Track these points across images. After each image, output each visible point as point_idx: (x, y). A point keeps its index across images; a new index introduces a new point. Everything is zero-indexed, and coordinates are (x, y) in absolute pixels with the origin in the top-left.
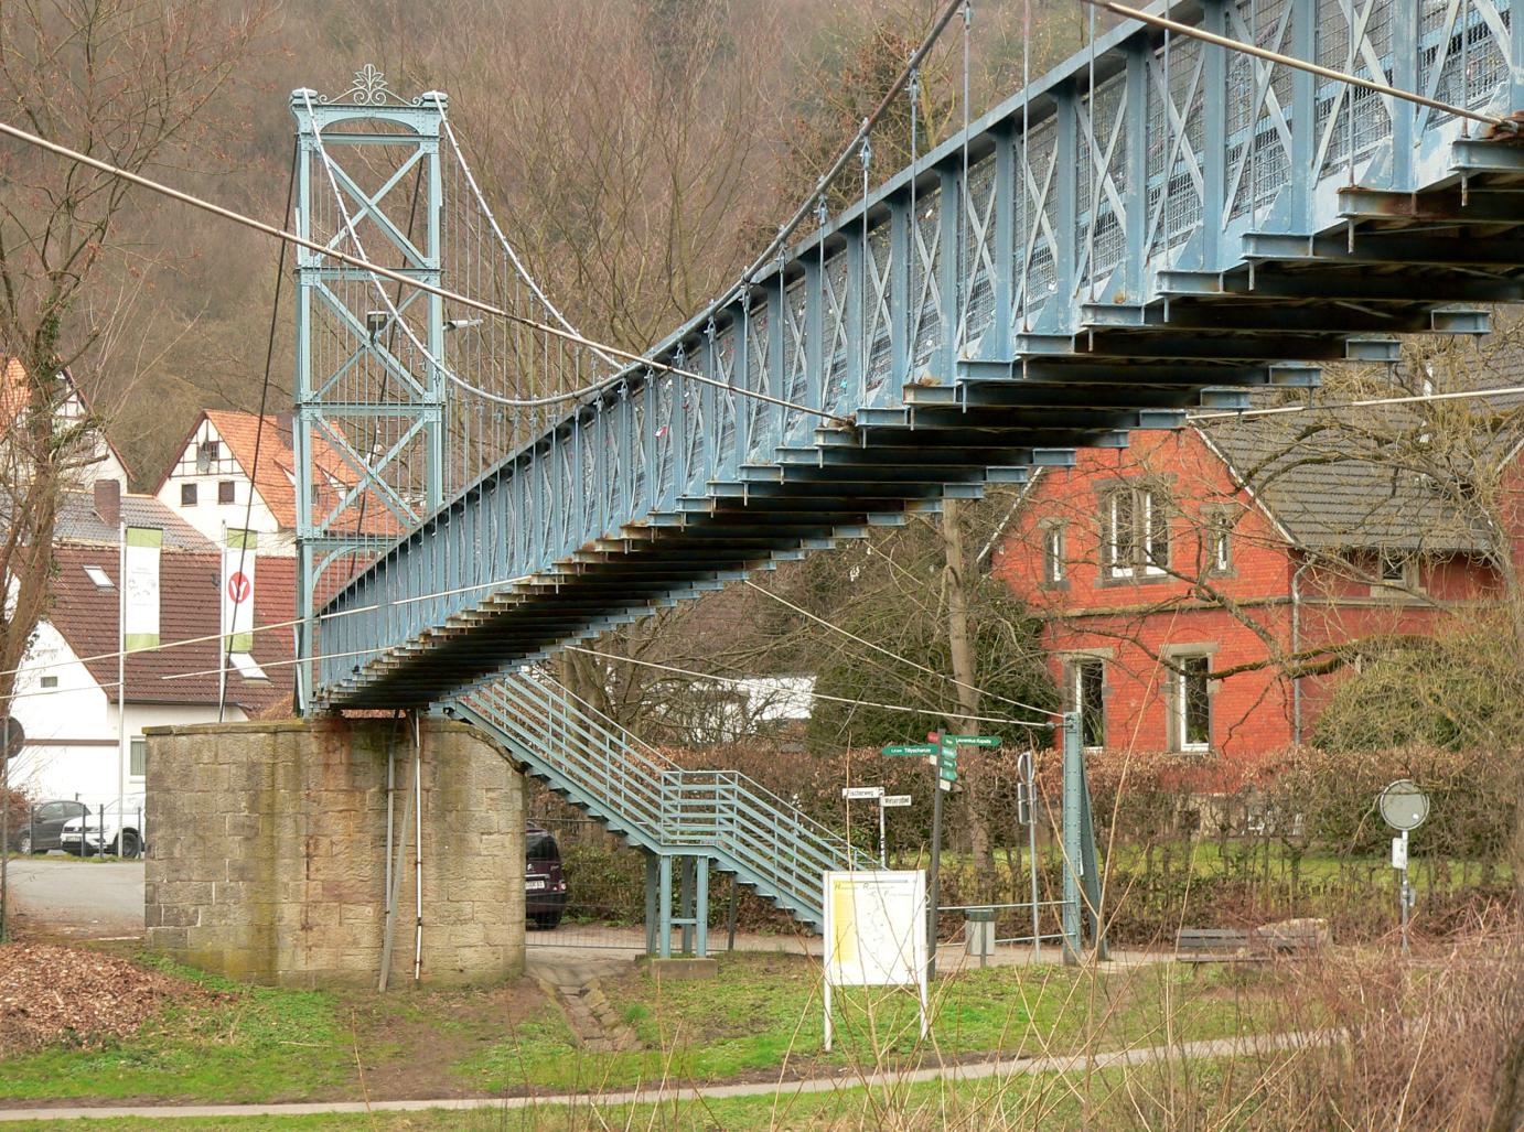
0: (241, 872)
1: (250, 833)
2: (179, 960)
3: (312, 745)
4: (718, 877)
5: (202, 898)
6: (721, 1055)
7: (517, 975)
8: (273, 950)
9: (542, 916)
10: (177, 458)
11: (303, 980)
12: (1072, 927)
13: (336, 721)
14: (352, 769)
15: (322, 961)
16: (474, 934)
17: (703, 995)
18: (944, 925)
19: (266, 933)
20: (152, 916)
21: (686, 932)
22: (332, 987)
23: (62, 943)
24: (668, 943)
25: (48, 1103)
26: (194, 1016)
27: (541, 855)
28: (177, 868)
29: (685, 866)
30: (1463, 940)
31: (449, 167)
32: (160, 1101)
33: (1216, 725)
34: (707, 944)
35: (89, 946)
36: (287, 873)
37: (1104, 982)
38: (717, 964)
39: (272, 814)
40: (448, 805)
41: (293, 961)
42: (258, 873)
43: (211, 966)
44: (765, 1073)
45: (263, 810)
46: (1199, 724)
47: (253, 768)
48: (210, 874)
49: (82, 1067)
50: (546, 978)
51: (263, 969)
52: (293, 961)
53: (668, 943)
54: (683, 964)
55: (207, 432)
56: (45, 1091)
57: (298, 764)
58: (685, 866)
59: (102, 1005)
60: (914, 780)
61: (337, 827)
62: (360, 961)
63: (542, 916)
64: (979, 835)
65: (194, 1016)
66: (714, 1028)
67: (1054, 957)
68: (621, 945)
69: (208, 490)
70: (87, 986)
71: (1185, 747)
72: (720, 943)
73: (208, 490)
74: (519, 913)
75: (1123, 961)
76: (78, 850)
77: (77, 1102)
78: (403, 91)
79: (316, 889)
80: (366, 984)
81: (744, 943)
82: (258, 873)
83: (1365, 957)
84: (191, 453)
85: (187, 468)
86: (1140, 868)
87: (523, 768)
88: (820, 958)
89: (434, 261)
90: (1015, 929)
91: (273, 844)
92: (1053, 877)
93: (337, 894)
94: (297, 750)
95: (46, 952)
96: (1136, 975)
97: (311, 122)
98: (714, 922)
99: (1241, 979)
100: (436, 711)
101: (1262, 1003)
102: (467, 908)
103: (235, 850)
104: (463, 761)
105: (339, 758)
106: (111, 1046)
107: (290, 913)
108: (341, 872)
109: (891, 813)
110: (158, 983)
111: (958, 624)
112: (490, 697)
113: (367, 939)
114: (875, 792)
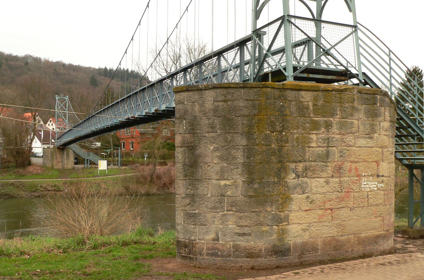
0: (51, 160)
1: (51, 157)
2: (46, 167)
3: (56, 150)
4: (90, 161)
5: (47, 162)
6: (91, 175)
7: (74, 169)
8: (53, 167)
9: (76, 163)
10: (48, 121)
11: (56, 169)
12: (119, 164)
13: (58, 148)
14: (60, 152)
15: (57, 167)
16: (70, 165)
17: (89, 170)
18: (108, 165)
19: (53, 165)
20: (43, 164)
21: (88, 165)
22: (58, 170)
23: (36, 166)
24: (86, 166)
25: (35, 179)
26: (47, 172)
27: (76, 159)
28: (45, 159)
29: (87, 160)
30: (149, 166)
31: (68, 102)
32: (44, 179)
33: (134, 147)
34: (89, 166)
35: (38, 166)
36: (54, 160)
37: (122, 169)
38: (90, 168)
39: (53, 155)
40: (68, 155)
41: (55, 167)
42: (52, 160)
43: (48, 168)
44: (93, 177)
45: (52, 155)
46: (132, 147)
47: (51, 152)
48: (48, 160)
49: (37, 176)
50: (76, 169)
51: (52, 168)
52: (55, 167)
53: (86, 166)
54: (87, 168)
55: (51, 119)
56: (35, 178)
57: (55, 151)
58: (87, 160)
59: (39, 171)
60: (107, 153)
61: (59, 157)
62: (60, 167)
63: (76, 163)
64: (113, 157)
65: (47, 172)
66: (90, 173)
67: (118, 167)
68: (82, 166)
69: (51, 124)
70: (38, 169)
71: (131, 149)
72: (90, 166)
73: (51, 124)
74: (74, 164)
75: (123, 167)
76: (38, 157)
77: (37, 179)
78: (65, 96)
79: (57, 162)
80: (60, 169)
81: (93, 166)
82: (52, 160)
83: (142, 167)
84: (49, 121)
85: (49, 122)
86: (125, 160)
87: (74, 152)
88: (98, 167)
89: (67, 110)
90: (114, 165)
91: (53, 158)
92: (118, 161)
93: (59, 162)
94: (55, 150)
95: (34, 167)
96: (124, 168)
97: (57, 98)
98: (90, 164)
99: (132, 169)
100: (67, 147)
101: (134, 171)
102: (69, 163)
103: (50, 158)
104: (69, 151)
105: (59, 151)
106: (40, 174)
107: (55, 163)
108: (59, 160)
109: (105, 155)
110: (44, 169)
111: (111, 140)
112: (73, 146)
113: (61, 166)
114: (104, 153)
